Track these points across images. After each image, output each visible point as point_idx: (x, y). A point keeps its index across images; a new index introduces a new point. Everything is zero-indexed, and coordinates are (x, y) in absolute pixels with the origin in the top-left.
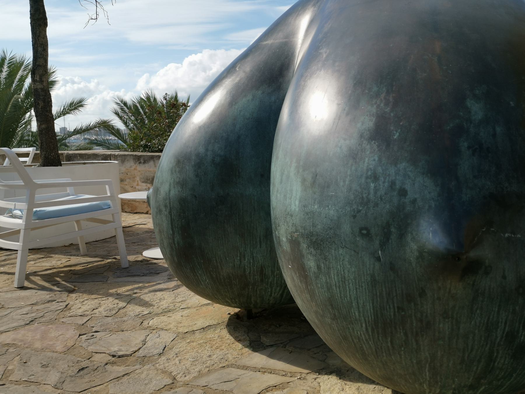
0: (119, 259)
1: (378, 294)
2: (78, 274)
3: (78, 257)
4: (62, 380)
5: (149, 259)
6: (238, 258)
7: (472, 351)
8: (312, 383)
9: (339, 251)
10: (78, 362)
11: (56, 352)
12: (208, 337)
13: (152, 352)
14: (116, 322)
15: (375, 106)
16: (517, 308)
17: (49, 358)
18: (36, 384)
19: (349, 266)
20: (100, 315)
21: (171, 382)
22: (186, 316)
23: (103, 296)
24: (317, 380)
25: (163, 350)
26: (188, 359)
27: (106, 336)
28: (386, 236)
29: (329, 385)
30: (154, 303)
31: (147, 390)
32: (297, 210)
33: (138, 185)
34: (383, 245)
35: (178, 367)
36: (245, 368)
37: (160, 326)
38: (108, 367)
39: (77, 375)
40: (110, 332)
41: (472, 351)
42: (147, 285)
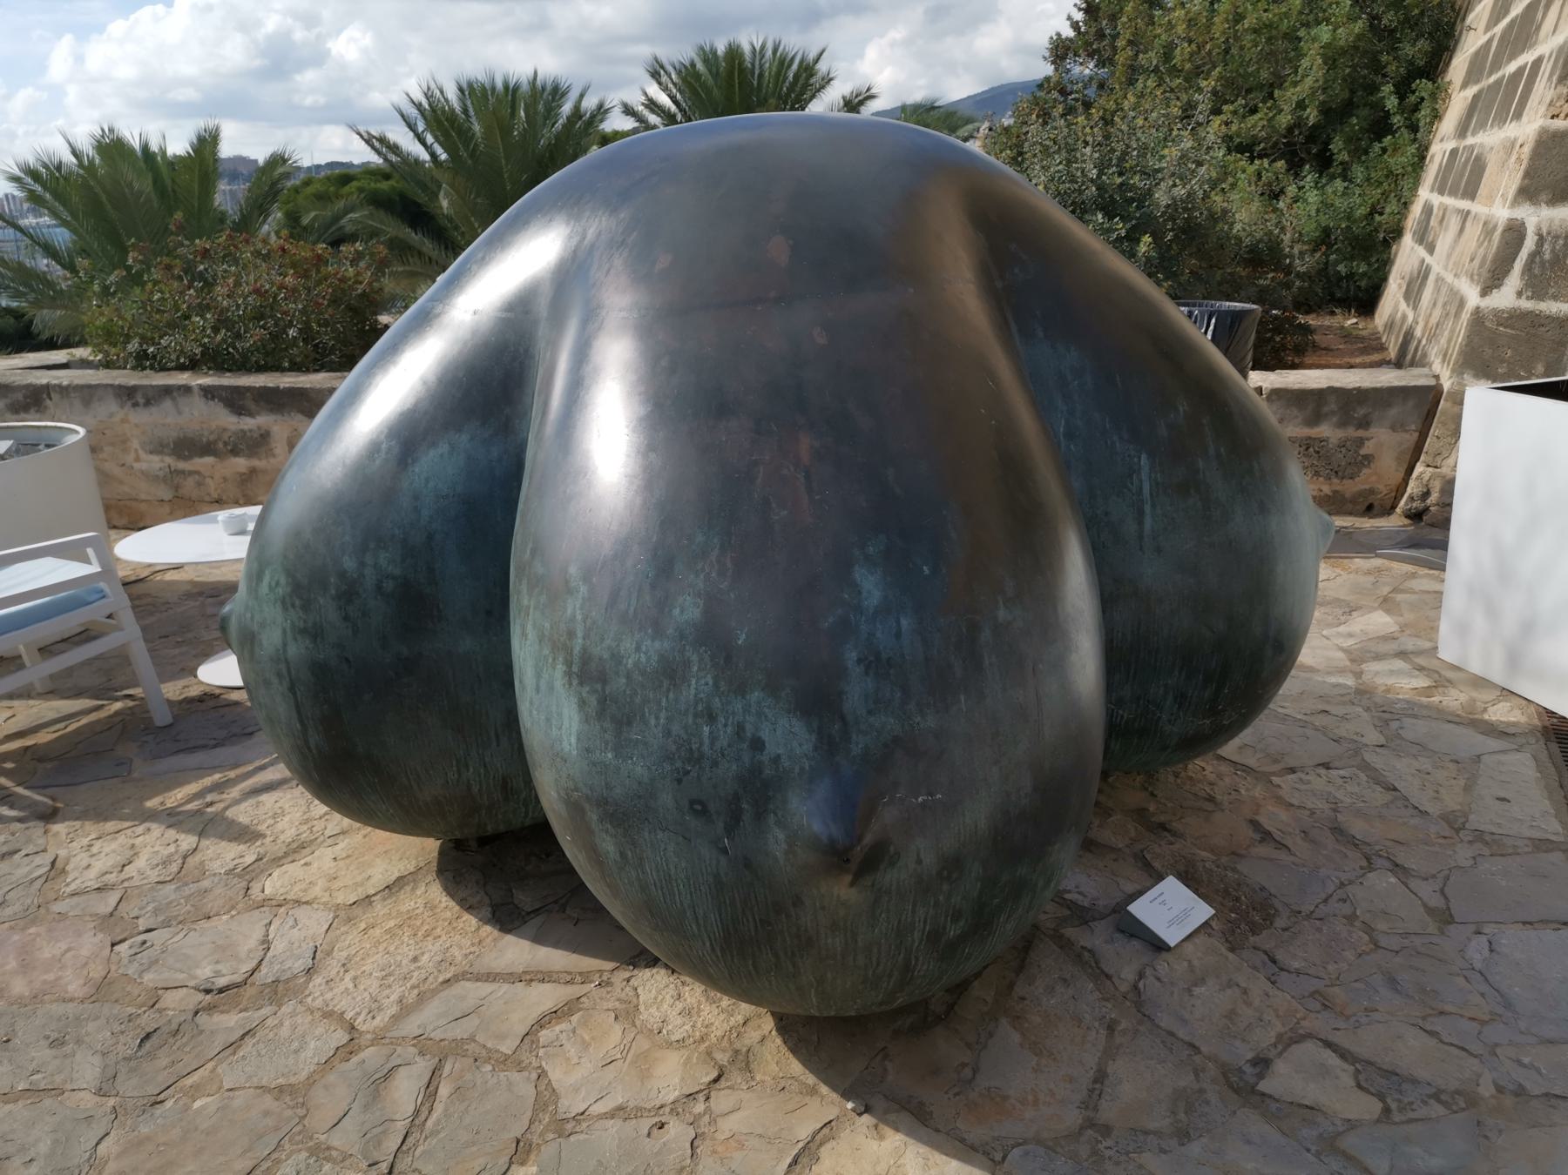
0: (142, 699)
1: (728, 902)
2: (51, 760)
3: (31, 702)
4: (110, 1073)
5: (218, 691)
6: (455, 769)
7: (878, 965)
8: (622, 990)
9: (656, 835)
10: (131, 1018)
11: (72, 1000)
12: (403, 908)
13: (290, 968)
14: (187, 898)
15: (702, 577)
16: (941, 898)
17: (59, 1020)
18: (53, 1092)
19: (676, 860)
20: (145, 881)
21: (346, 1038)
22: (343, 859)
23: (132, 823)
24: (630, 983)
25: (314, 958)
26: (371, 974)
27: (175, 939)
28: (735, 818)
29: (654, 991)
30: (262, 828)
31: (301, 1066)
32: (575, 753)
33: (137, 459)
34: (730, 830)
35: (354, 998)
36: (490, 977)
37: (292, 893)
38: (202, 1019)
39: (140, 1054)
40: (180, 926)
41: (878, 965)
42: (232, 774)
